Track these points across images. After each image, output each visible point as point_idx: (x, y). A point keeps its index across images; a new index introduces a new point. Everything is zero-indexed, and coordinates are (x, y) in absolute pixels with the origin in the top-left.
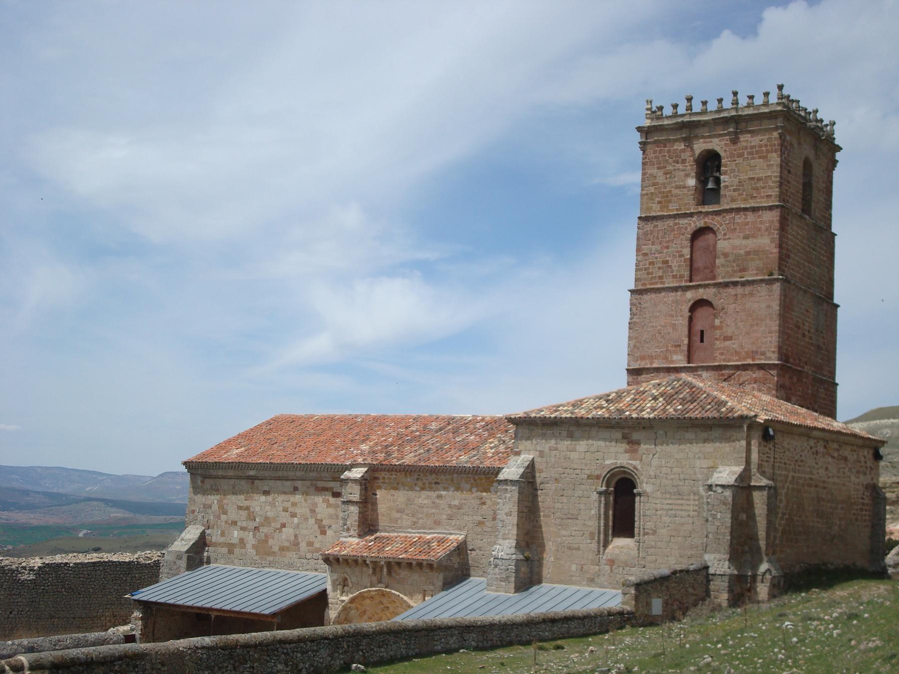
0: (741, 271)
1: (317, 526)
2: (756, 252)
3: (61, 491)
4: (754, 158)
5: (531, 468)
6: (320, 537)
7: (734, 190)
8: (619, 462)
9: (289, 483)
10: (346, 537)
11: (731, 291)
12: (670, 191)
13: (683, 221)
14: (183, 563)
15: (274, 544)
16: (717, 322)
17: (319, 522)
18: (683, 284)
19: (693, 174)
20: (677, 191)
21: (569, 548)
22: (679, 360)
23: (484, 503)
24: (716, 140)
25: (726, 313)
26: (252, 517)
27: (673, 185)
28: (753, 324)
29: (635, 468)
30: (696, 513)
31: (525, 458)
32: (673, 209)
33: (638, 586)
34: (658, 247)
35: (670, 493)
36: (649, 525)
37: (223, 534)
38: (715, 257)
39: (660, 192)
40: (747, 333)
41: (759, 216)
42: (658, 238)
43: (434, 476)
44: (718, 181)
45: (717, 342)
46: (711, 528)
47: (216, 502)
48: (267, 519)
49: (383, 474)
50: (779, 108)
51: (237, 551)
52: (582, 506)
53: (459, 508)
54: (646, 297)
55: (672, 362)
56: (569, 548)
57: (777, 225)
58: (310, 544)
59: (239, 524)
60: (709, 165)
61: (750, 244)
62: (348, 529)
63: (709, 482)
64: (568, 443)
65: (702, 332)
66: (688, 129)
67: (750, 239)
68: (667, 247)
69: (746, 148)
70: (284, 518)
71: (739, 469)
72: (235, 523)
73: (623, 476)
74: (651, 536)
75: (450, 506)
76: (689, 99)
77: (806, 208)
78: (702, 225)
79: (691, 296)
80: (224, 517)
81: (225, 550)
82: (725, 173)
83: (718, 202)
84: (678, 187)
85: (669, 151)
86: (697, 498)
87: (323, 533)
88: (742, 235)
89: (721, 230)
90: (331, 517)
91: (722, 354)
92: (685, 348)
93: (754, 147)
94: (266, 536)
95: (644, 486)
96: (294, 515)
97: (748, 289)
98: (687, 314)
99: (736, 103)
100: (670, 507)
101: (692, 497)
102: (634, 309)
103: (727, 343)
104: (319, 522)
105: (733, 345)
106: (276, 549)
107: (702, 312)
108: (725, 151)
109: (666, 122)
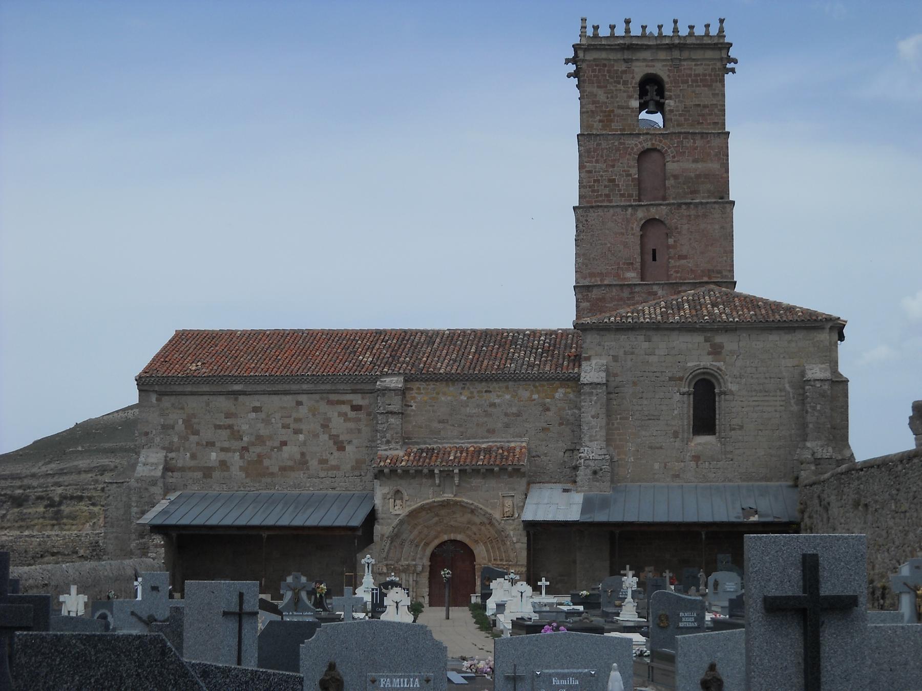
0: (692, 193)
1: (331, 442)
4: (699, 86)
6: (336, 454)
7: (680, 115)
8: (702, 364)
9: (289, 397)
10: (386, 450)
12: (613, 111)
16: (671, 241)
17: (335, 439)
20: (620, 112)
21: (651, 448)
22: (632, 276)
23: (548, 409)
25: (679, 233)
26: (236, 435)
27: (616, 105)
29: (718, 369)
30: (783, 408)
35: (755, 390)
37: (193, 457)
38: (665, 178)
39: (602, 111)
41: (708, 142)
42: (602, 156)
43: (484, 384)
45: (672, 261)
47: (180, 421)
49: (417, 384)
51: (216, 474)
52: (664, 408)
53: (518, 415)
55: (625, 279)
56: (651, 448)
58: (323, 462)
59: (218, 444)
65: (654, 251)
68: (613, 166)
69: (690, 75)
70: (284, 435)
72: (211, 444)
73: (697, 379)
74: (739, 432)
75: (506, 415)
76: (628, 22)
78: (649, 146)
79: (640, 214)
80: (193, 438)
81: (199, 475)
82: (670, 98)
84: (620, 107)
86: (783, 394)
87: (341, 448)
88: (691, 158)
91: (677, 272)
92: (638, 265)
93: (698, 75)
94: (259, 456)
96: (297, 432)
99: (676, 30)
100: (757, 403)
101: (778, 393)
102: (580, 226)
103: (683, 262)
108: (669, 76)
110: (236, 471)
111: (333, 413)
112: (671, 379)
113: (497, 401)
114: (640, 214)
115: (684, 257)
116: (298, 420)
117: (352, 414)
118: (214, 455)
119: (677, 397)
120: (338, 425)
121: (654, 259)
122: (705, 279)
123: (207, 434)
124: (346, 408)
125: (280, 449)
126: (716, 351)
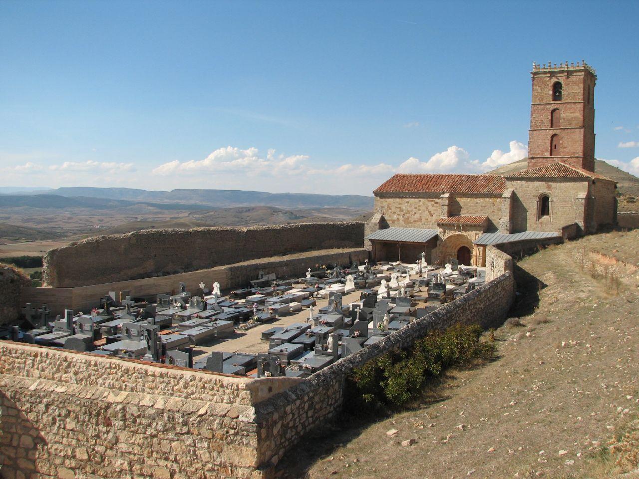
2: (575, 118)
3: (125, 199)
5: (514, 194)
13: (549, 106)
14: (378, 227)
15: (411, 220)
17: (430, 212)
18: (549, 128)
19: (551, 90)
22: (547, 154)
26: (402, 210)
28: (573, 144)
31: (510, 190)
32: (544, 102)
36: (555, 211)
40: (572, 146)
48: (408, 211)
55: (545, 155)
57: (582, 109)
60: (557, 87)
61: (573, 115)
62: (444, 214)
65: (555, 145)
67: (572, 113)
70: (415, 210)
77: (588, 102)
79: (551, 133)
80: (390, 211)
83: (560, 100)
84: (546, 94)
85: (542, 81)
90: (434, 210)
92: (550, 151)
94: (408, 217)
96: (419, 210)
97: (572, 130)
104: (430, 212)
106: (412, 221)
110: (401, 221)
111: (429, 204)
113: (479, 202)
115: (566, 148)
116: (419, 206)
117: (435, 205)
118: (395, 216)
120: (431, 208)
122: (572, 156)
123: (393, 209)
124: (433, 203)
125: (414, 215)
126: (549, 187)
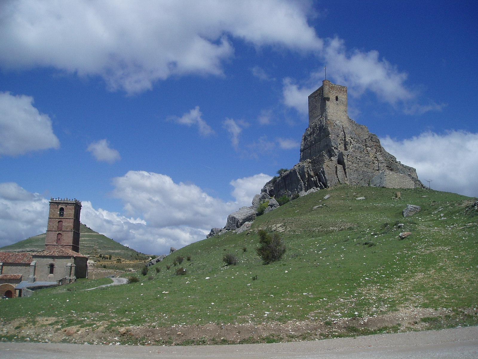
11: (65, 232)
13: (57, 219)
16: (62, 237)
24: (63, 206)
33: (59, 281)
34: (52, 223)
44: (63, 213)
46: (67, 272)
50: (75, 202)
54: (49, 232)
57: (73, 222)
60: (62, 210)
63: (67, 265)
64: (43, 259)
65: (59, 239)
66: (58, 203)
71: (71, 263)
84: (56, 213)
89: (64, 221)
95: (56, 266)
98: (57, 235)
103: (64, 241)
105: (65, 241)
107: (60, 235)
109: (54, 201)
112: (46, 265)
114: (57, 232)
119: (47, 268)
121: (59, 240)
